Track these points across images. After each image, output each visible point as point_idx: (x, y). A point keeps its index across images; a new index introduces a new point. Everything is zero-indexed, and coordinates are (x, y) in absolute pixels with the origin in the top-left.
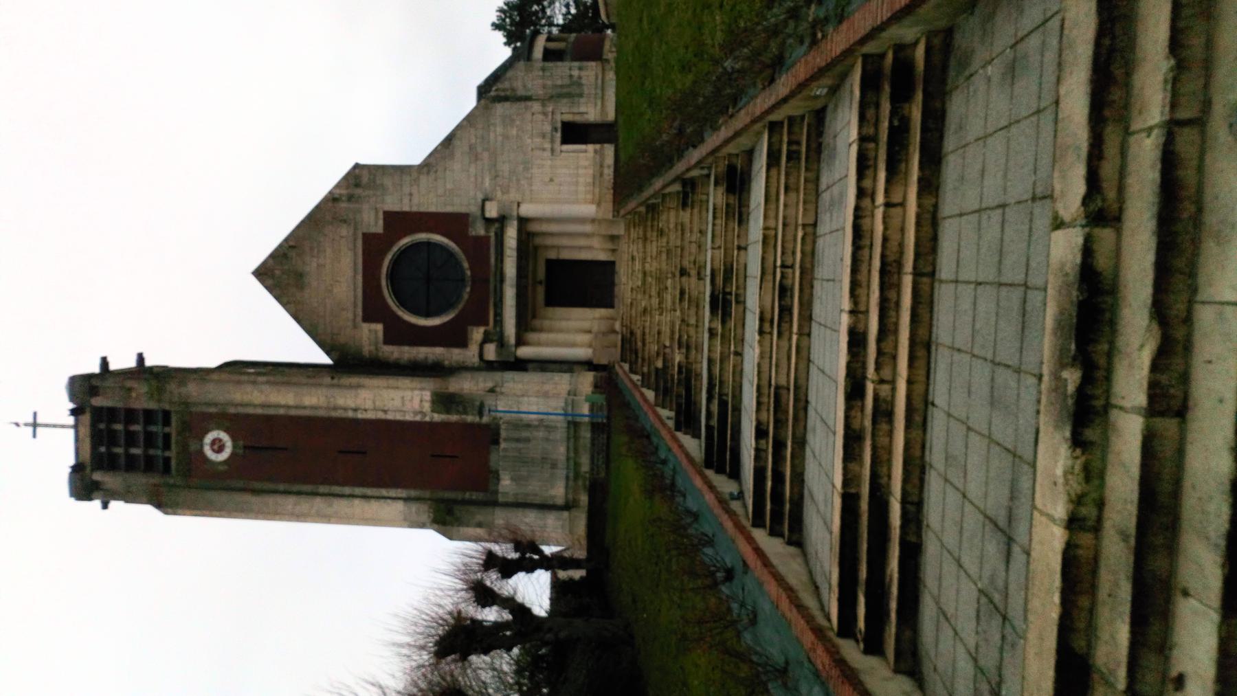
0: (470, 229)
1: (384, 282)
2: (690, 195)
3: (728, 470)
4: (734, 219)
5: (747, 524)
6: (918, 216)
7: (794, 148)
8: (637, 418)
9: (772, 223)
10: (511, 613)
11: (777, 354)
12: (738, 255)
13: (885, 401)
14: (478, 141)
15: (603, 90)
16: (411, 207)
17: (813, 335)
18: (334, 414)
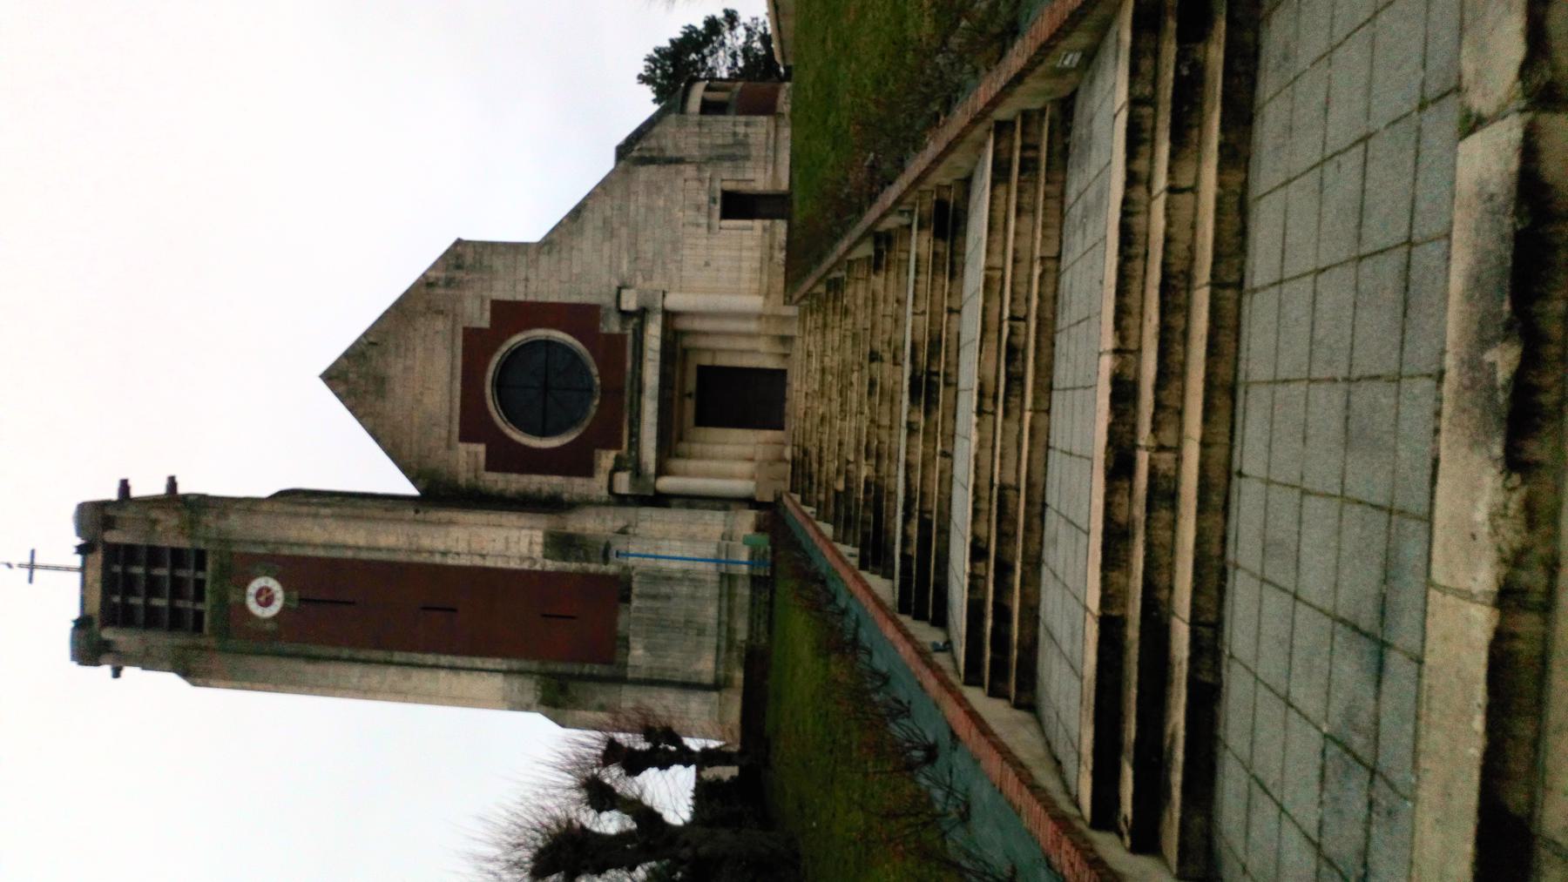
0: (601, 325)
1: (488, 391)
2: (885, 253)
3: (930, 614)
4: (944, 273)
5: (957, 681)
6: (1219, 201)
7: (1030, 154)
8: (809, 560)
9: (997, 261)
10: (635, 819)
11: (1002, 439)
12: (949, 319)
13: (1165, 476)
14: (615, 212)
15: (776, 150)
16: (526, 295)
17: (1053, 410)
18: (417, 558)
